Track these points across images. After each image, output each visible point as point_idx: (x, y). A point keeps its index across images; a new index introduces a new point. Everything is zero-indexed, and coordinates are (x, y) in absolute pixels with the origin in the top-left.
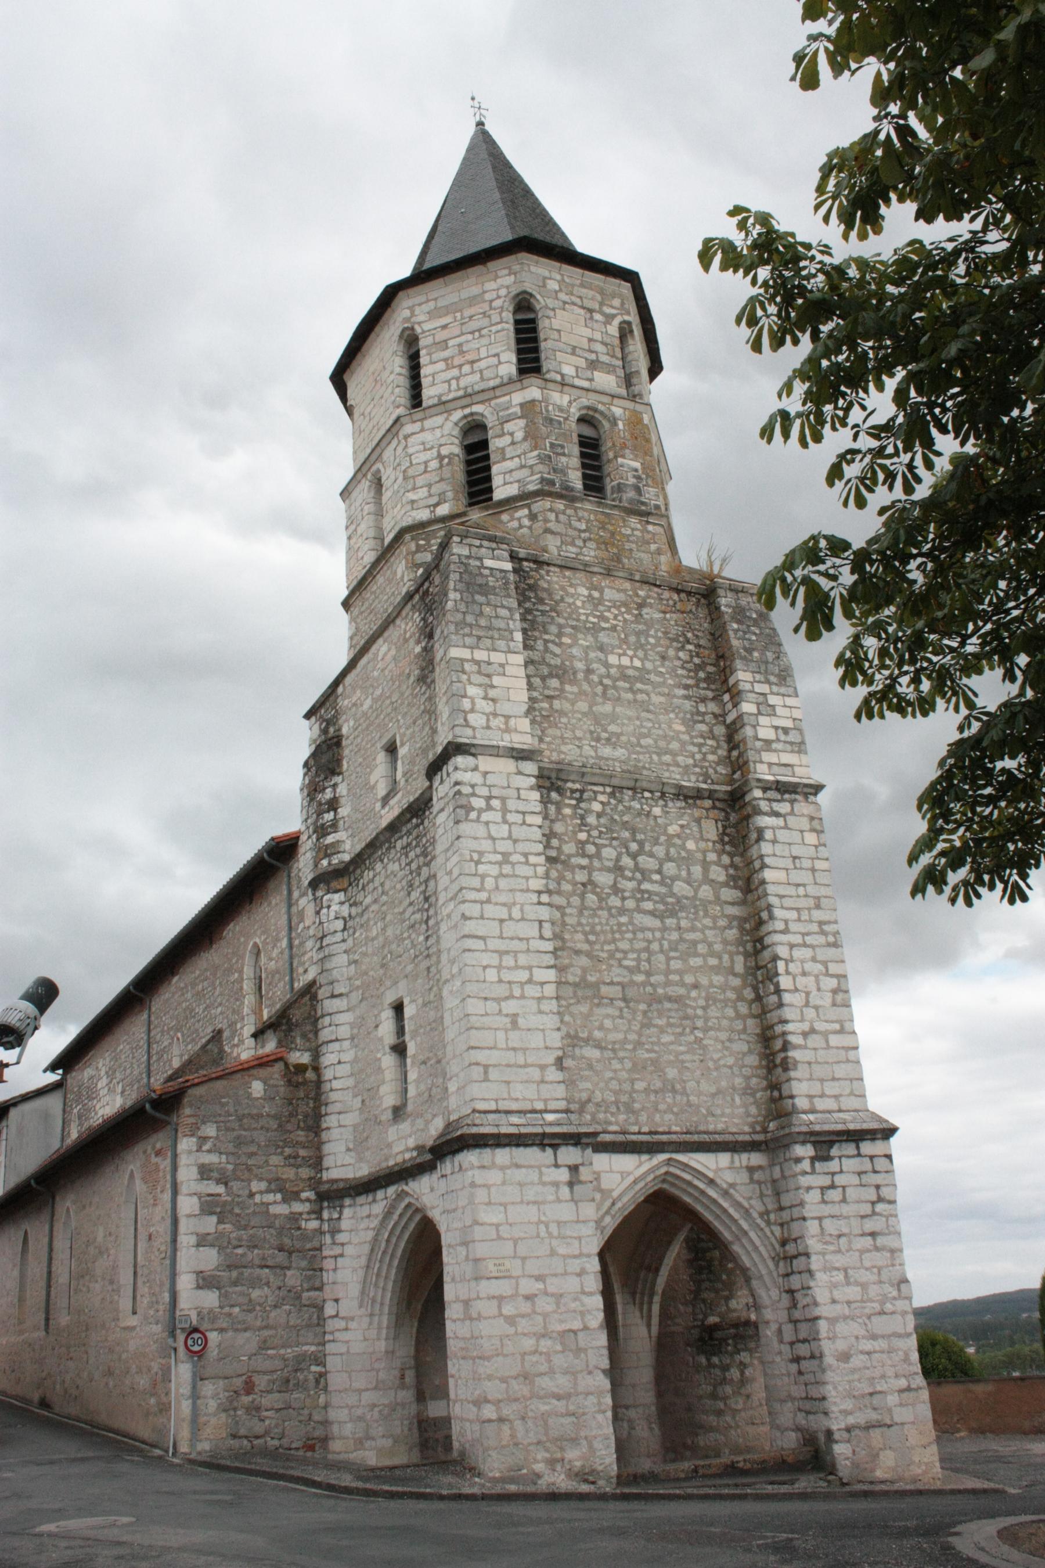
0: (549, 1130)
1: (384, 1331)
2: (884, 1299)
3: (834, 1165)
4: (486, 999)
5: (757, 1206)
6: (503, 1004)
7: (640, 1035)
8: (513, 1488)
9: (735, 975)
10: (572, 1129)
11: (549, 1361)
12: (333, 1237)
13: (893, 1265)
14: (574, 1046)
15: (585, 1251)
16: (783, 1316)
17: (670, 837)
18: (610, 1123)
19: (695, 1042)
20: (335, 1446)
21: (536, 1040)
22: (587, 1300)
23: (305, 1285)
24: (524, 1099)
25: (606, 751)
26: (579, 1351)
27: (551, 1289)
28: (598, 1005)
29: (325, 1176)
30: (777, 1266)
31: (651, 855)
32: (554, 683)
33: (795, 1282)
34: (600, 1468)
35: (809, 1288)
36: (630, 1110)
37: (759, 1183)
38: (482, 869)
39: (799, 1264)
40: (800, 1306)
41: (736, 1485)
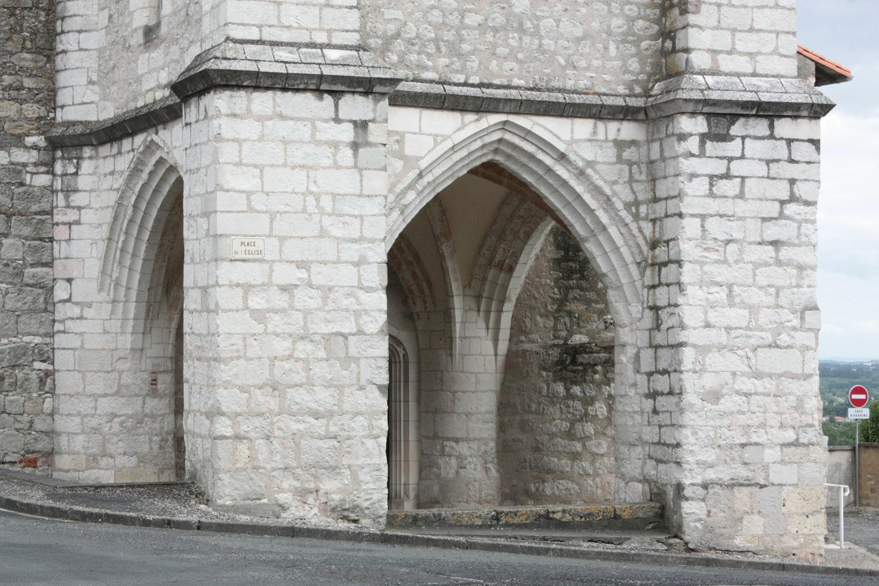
0: (327, 71)
1: (131, 323)
3: (733, 148)
5: (623, 193)
8: (244, 519)
10: (362, 73)
12: (67, 198)
13: (799, 286)
15: (367, 234)
16: (643, 339)
18: (426, 68)
20: (63, 462)
22: (364, 297)
23: (29, 259)
24: (300, 28)
26: (348, 360)
27: (317, 280)
29: (61, 116)
30: (642, 275)
33: (662, 296)
34: (366, 504)
35: (676, 306)
36: (455, 51)
37: (630, 164)
39: (668, 273)
40: (664, 327)
41: (544, 539)
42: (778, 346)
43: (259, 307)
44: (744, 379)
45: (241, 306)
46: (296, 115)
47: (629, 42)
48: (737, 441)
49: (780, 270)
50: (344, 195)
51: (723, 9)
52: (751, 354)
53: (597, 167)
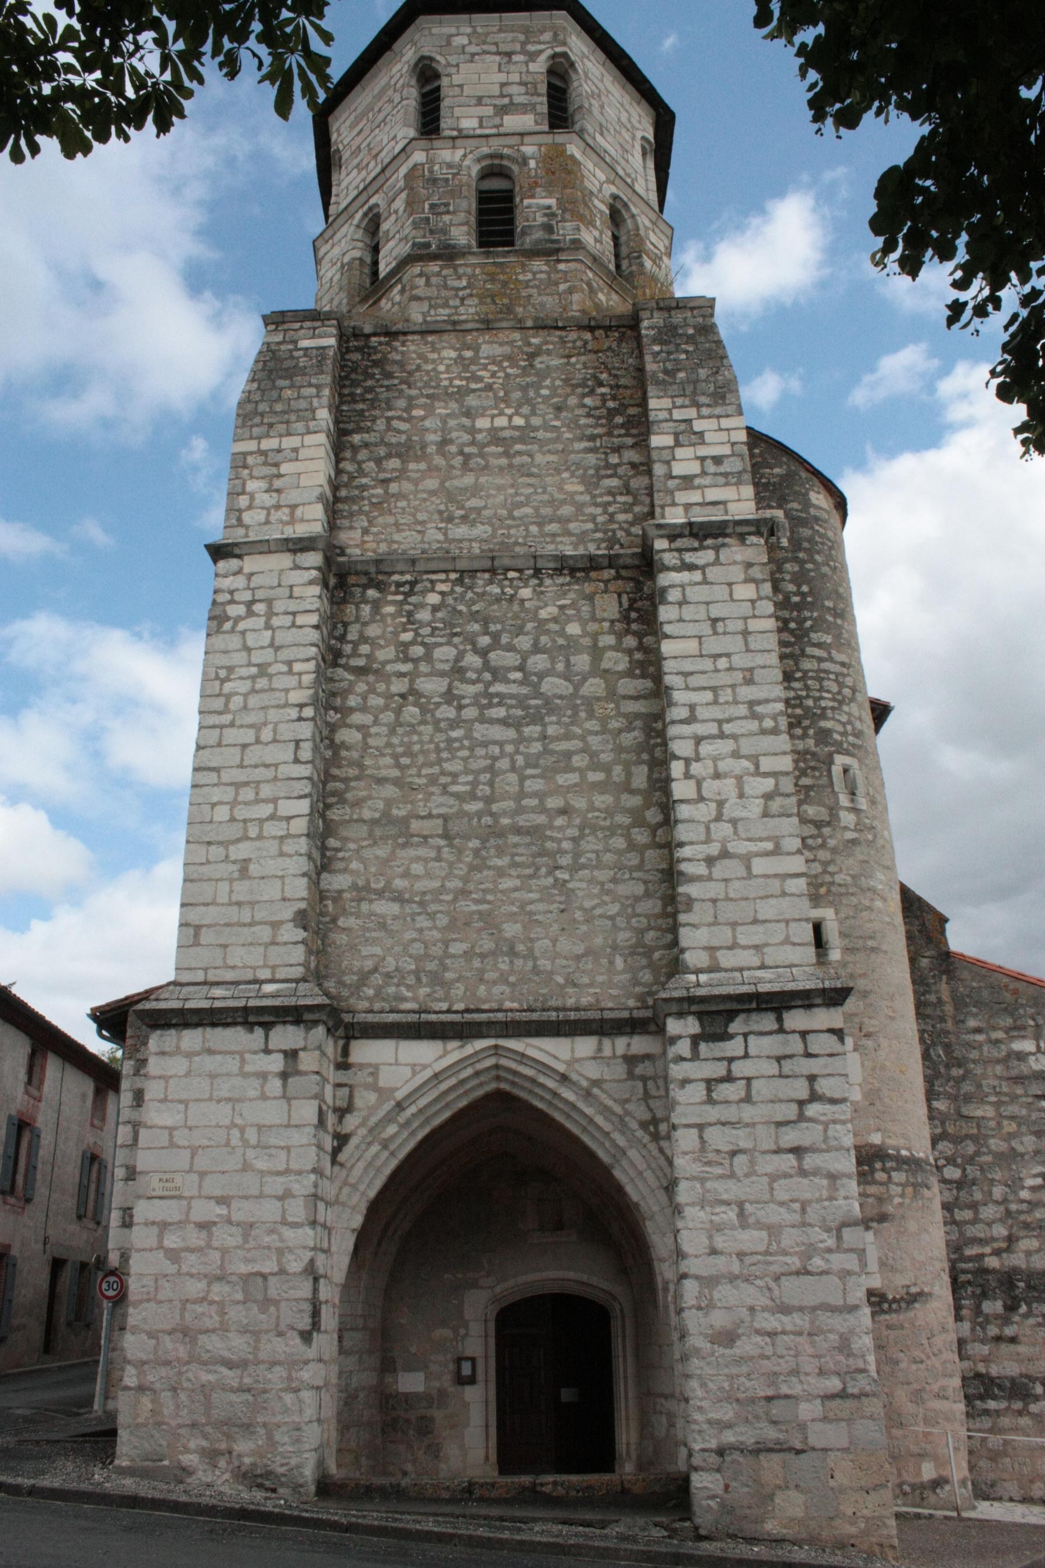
2: (809, 1251)
3: (734, 1047)
4: (209, 843)
6: (232, 848)
7: (466, 880)
9: (633, 792)
10: (291, 1002)
11: (222, 1313)
13: (831, 1198)
14: (360, 900)
15: (294, 1166)
17: (542, 622)
18: (405, 999)
19: (554, 886)
21: (272, 891)
22: (288, 1233)
24: (245, 967)
25: (460, 531)
26: (267, 1302)
28: (404, 846)
31: (510, 648)
32: (394, 463)
36: (436, 979)
38: (228, 687)
42: (808, 1273)
43: (174, 1246)
44: (766, 1315)
45: (155, 1245)
46: (225, 1048)
47: (639, 954)
48: (762, 1394)
49: (805, 1181)
50: (270, 1126)
51: (718, 904)
52: (772, 1285)
53: (605, 1086)
